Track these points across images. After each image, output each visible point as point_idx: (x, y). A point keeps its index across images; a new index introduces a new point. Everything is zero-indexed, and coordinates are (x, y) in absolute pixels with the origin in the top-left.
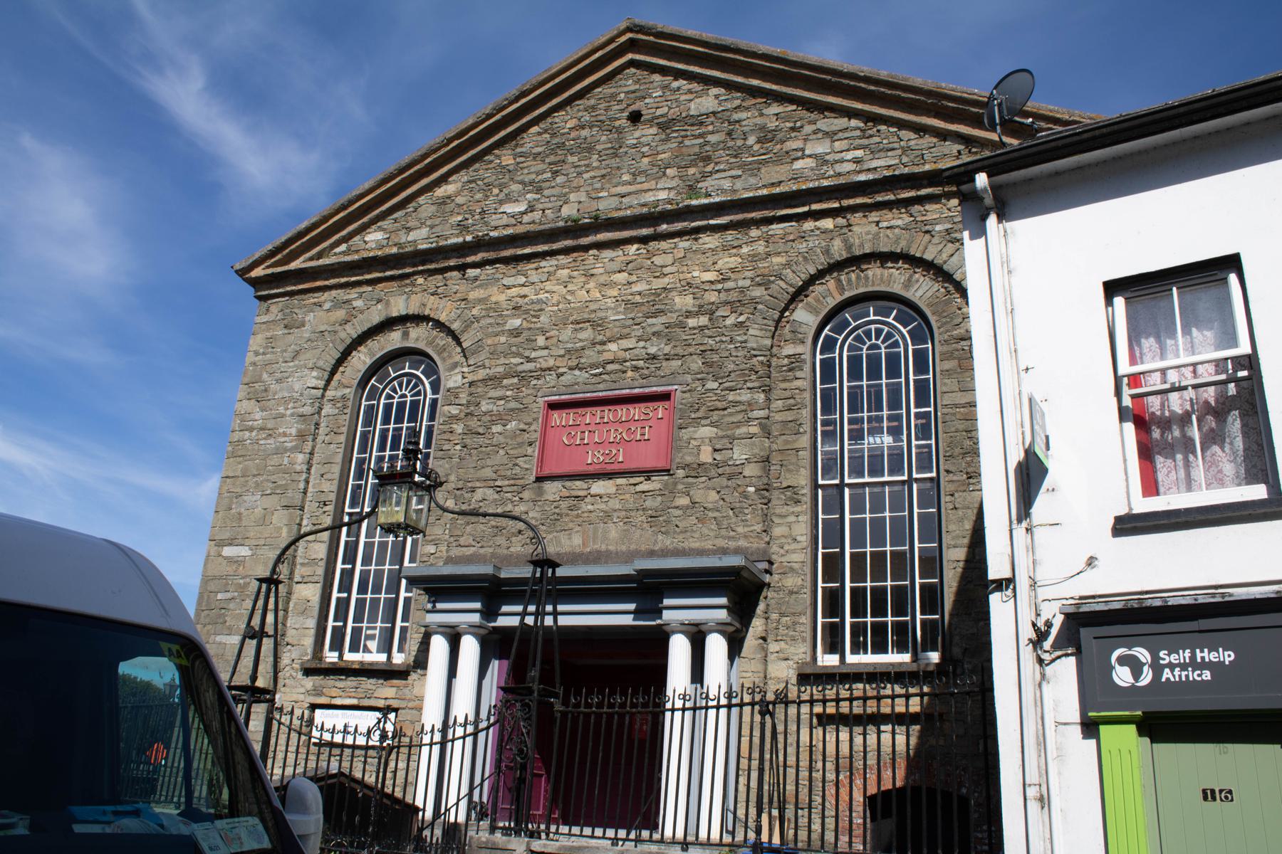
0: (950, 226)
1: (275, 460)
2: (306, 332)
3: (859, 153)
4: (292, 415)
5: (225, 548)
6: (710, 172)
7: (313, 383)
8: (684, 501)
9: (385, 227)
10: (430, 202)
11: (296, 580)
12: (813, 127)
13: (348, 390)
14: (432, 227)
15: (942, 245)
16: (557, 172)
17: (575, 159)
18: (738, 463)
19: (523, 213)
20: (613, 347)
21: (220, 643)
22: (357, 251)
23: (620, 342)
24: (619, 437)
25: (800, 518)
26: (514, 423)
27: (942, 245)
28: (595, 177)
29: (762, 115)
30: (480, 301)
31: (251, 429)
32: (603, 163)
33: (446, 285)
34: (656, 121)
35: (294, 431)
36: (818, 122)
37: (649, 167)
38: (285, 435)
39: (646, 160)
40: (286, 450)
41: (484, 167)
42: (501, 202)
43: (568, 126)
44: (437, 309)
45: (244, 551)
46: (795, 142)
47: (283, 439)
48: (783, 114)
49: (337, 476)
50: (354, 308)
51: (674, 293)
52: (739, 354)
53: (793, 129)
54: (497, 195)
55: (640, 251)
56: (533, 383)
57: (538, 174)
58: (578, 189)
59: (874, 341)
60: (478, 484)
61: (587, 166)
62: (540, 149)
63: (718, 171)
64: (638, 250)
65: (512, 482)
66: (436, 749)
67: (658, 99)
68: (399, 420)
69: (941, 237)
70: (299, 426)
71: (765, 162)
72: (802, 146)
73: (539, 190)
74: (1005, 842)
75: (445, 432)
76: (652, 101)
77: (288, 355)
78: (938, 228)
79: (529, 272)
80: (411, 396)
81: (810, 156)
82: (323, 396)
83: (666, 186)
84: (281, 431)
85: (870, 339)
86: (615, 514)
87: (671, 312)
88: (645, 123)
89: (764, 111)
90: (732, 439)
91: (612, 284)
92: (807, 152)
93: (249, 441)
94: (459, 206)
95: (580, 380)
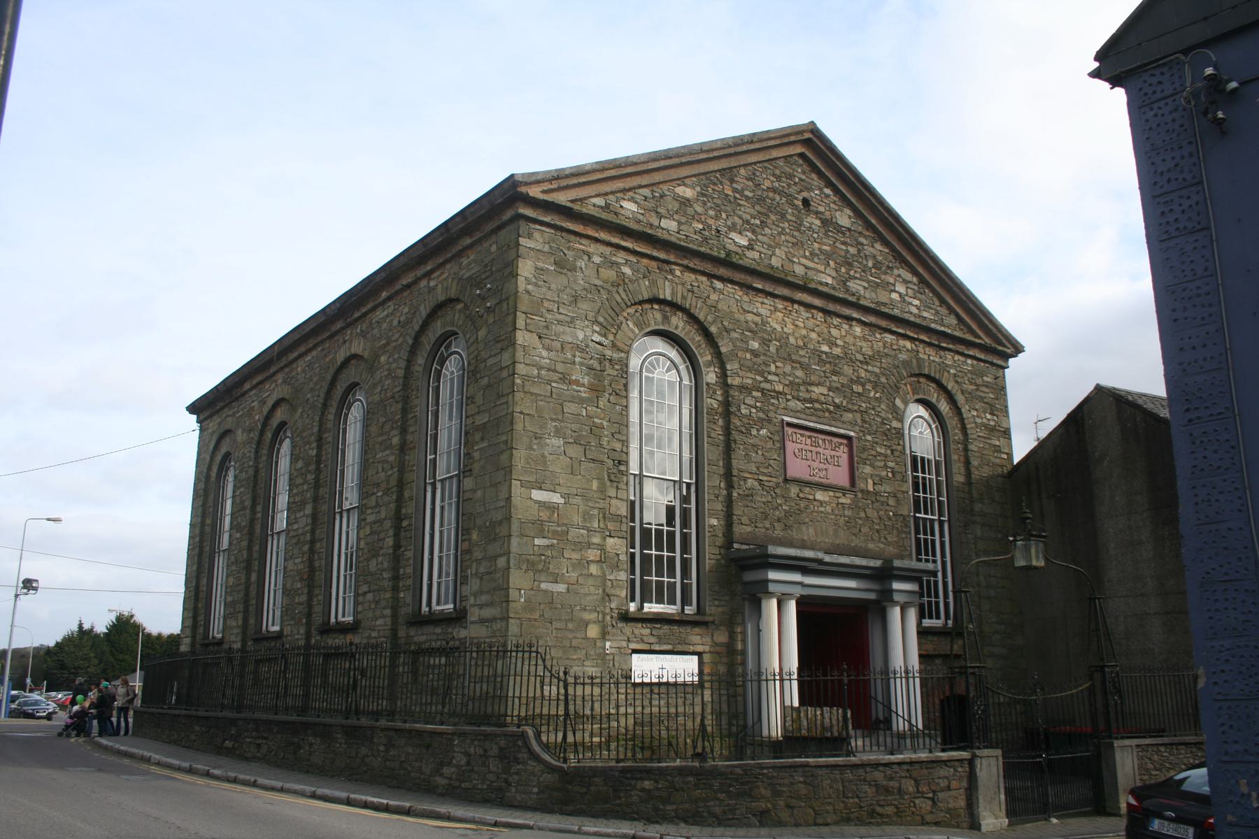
21: (546, 591)
60: (748, 476)
65: (769, 479)
66: (778, 682)
74: (1146, 245)
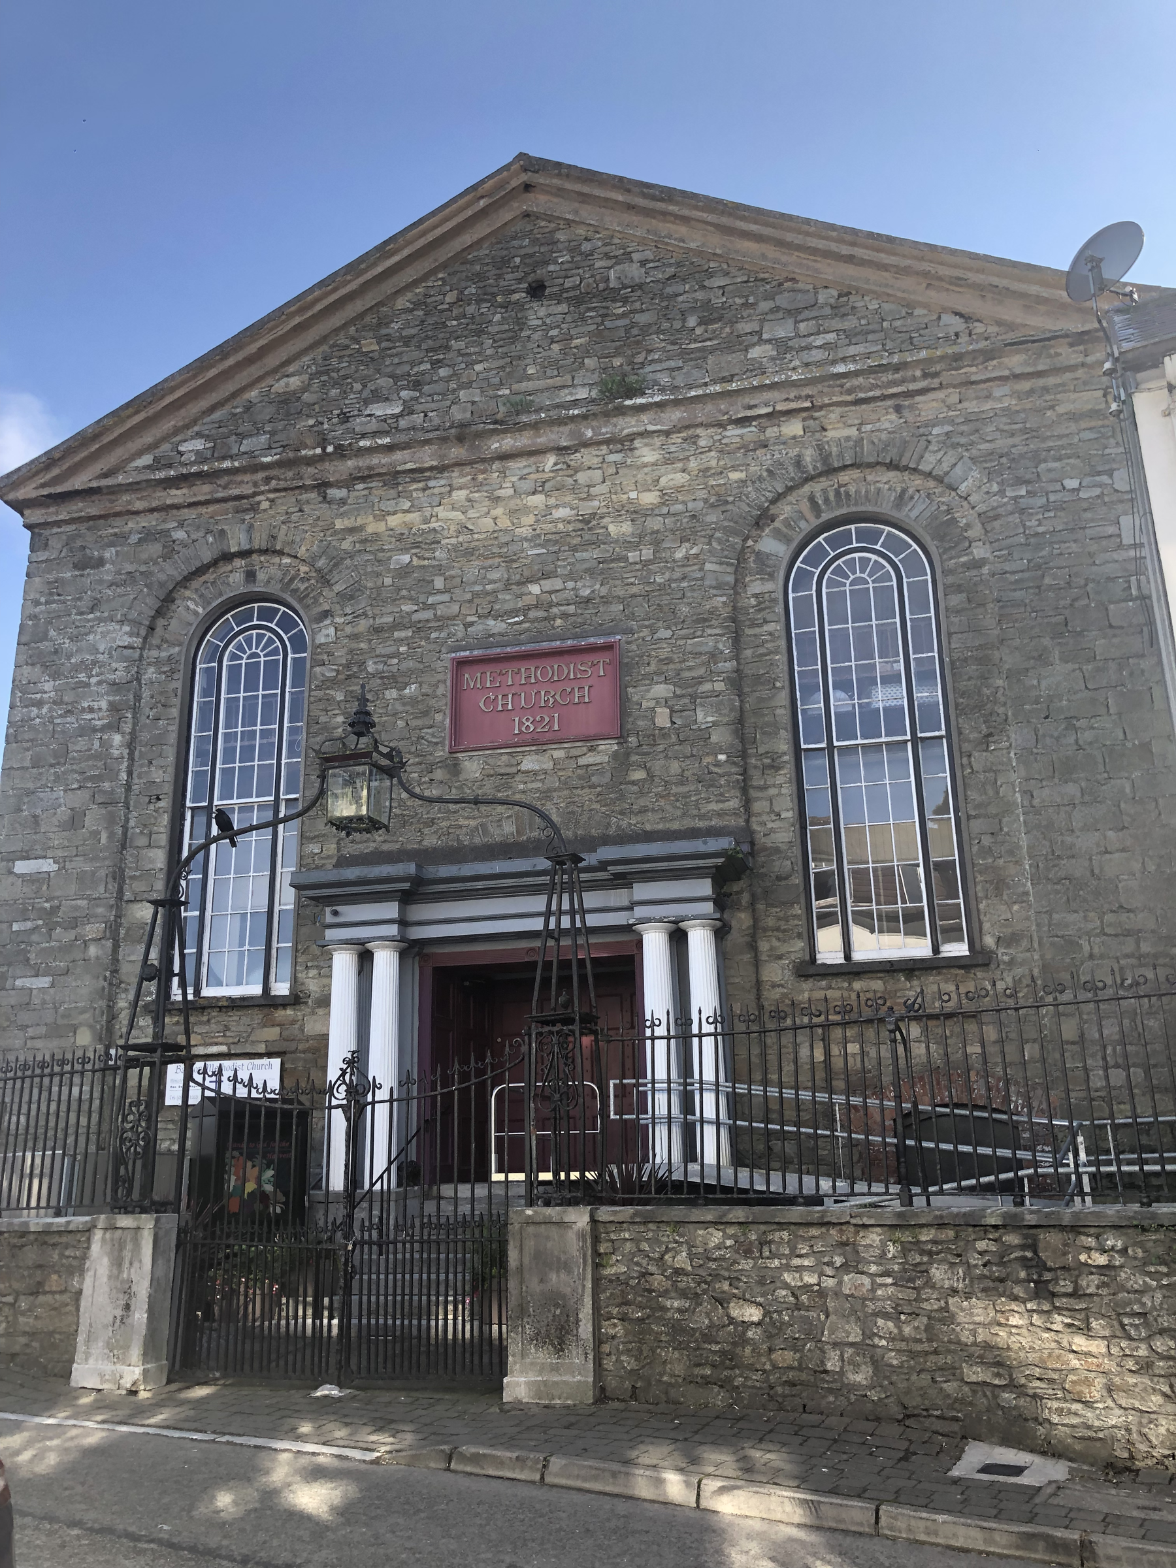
0: (950, 428)
1: (81, 744)
2: (108, 572)
3: (831, 337)
4: (99, 683)
5: (17, 863)
6: (642, 363)
7: (127, 640)
8: (639, 775)
9: (207, 432)
10: (266, 399)
11: (125, 898)
12: (770, 304)
13: (177, 649)
14: (272, 433)
15: (942, 452)
16: (439, 361)
17: (462, 344)
18: (703, 726)
19: (396, 417)
20: (535, 589)
21: (22, 988)
22: (170, 466)
23: (542, 582)
24: (552, 700)
25: (784, 791)
26: (413, 686)
27: (942, 452)
28: (492, 369)
29: (703, 287)
30: (351, 530)
31: (39, 704)
32: (500, 350)
33: (301, 510)
34: (565, 295)
35: (104, 705)
36: (777, 297)
37: (561, 356)
38: (91, 710)
39: (556, 347)
40: (94, 730)
41: (337, 354)
42: (367, 402)
43: (448, 299)
44: (293, 542)
45: (48, 866)
46: (749, 325)
47: (89, 716)
48: (731, 287)
49: (171, 759)
50: (174, 541)
51: (606, 520)
52: (695, 595)
53: (746, 305)
54: (360, 392)
55: (558, 467)
56: (433, 635)
57: (412, 364)
58: (468, 385)
59: (858, 574)
61: (480, 353)
62: (413, 331)
63: (652, 361)
64: (555, 464)
67: (565, 266)
68: (251, 686)
69: (938, 442)
70: (111, 698)
71: (713, 350)
72: (758, 329)
73: (417, 385)
75: (320, 700)
76: (557, 268)
77: (84, 604)
78: (935, 431)
79: (415, 494)
80: (265, 656)
81: (769, 341)
82: (141, 656)
83: (586, 381)
84: (85, 705)
85: (854, 573)
86: (555, 794)
87: (605, 543)
88: (551, 297)
89: (706, 283)
90: (693, 697)
91: (526, 510)
92: (765, 336)
93: (38, 720)
94: (311, 405)
95: (495, 631)
